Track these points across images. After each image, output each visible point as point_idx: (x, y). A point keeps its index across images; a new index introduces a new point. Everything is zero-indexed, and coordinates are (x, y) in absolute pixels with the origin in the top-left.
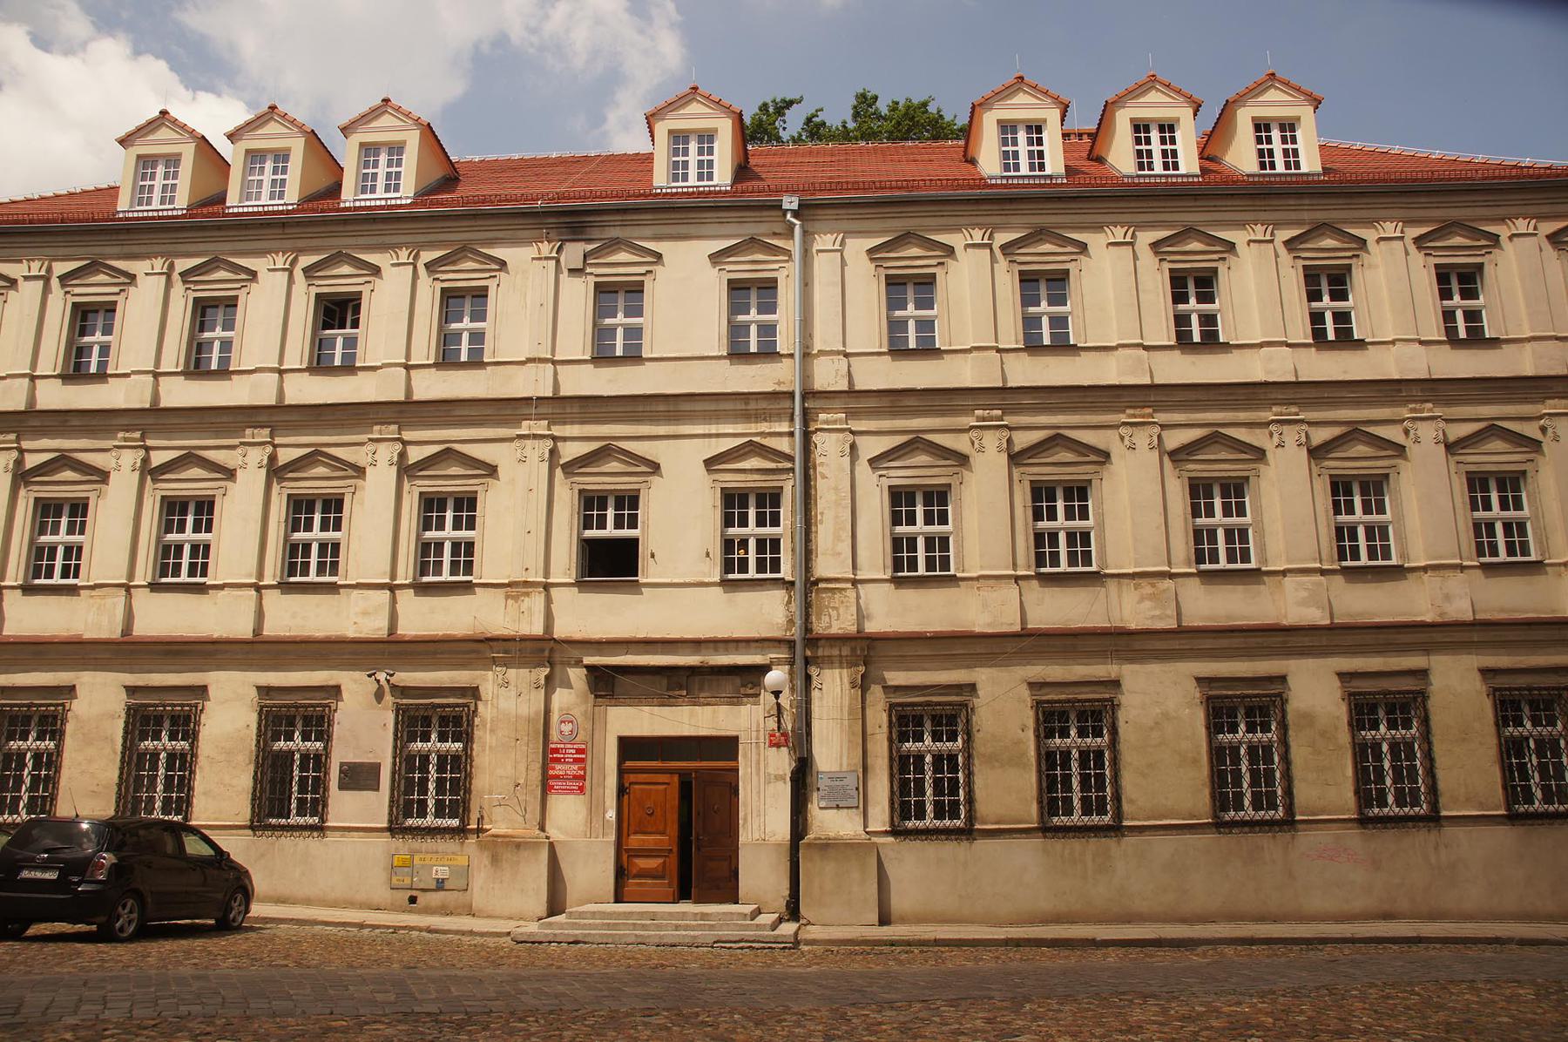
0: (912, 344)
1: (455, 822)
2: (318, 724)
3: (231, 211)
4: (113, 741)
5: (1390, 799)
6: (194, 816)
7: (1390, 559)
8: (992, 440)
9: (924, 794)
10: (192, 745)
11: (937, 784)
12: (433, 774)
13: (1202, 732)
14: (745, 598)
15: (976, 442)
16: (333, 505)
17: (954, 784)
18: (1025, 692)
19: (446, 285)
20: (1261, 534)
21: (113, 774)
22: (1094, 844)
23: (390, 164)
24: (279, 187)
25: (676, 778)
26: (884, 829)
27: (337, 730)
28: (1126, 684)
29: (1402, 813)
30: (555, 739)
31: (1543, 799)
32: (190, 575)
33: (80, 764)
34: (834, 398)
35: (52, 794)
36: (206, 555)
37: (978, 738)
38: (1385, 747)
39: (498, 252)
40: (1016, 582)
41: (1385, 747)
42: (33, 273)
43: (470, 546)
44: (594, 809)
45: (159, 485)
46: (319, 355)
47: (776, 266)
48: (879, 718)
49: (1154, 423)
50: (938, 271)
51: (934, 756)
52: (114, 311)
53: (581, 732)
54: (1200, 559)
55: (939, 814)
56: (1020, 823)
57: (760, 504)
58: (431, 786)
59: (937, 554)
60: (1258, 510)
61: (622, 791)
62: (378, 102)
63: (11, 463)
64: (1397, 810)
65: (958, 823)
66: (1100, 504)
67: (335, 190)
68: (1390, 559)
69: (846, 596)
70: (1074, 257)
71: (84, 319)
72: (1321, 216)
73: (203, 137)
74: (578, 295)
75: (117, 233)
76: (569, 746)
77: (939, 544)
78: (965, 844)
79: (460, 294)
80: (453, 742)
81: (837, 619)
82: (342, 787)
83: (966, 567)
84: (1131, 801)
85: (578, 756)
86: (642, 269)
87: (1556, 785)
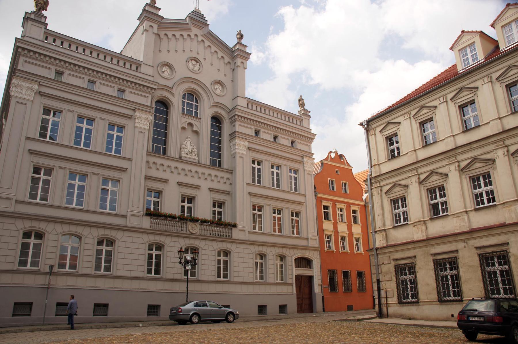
0: (473, 126)
3: (460, 72)
5: (451, 294)
8: (453, 167)
16: (487, 176)
18: (431, 258)
23: (471, 52)
24: (475, 57)
29: (455, 299)
31: (504, 293)
35: (460, 289)
36: (446, 205)
38: (449, 277)
41: (449, 277)
43: (492, 191)
46: (514, 107)
52: (397, 135)
55: (506, 293)
62: (460, 33)
63: (379, 191)
64: (454, 298)
67: (497, 47)
68: (484, 204)
70: (433, 111)
72: (460, 85)
73: (481, 31)
75: (466, 76)
79: (514, 84)
86: (431, 113)
87: (508, 287)
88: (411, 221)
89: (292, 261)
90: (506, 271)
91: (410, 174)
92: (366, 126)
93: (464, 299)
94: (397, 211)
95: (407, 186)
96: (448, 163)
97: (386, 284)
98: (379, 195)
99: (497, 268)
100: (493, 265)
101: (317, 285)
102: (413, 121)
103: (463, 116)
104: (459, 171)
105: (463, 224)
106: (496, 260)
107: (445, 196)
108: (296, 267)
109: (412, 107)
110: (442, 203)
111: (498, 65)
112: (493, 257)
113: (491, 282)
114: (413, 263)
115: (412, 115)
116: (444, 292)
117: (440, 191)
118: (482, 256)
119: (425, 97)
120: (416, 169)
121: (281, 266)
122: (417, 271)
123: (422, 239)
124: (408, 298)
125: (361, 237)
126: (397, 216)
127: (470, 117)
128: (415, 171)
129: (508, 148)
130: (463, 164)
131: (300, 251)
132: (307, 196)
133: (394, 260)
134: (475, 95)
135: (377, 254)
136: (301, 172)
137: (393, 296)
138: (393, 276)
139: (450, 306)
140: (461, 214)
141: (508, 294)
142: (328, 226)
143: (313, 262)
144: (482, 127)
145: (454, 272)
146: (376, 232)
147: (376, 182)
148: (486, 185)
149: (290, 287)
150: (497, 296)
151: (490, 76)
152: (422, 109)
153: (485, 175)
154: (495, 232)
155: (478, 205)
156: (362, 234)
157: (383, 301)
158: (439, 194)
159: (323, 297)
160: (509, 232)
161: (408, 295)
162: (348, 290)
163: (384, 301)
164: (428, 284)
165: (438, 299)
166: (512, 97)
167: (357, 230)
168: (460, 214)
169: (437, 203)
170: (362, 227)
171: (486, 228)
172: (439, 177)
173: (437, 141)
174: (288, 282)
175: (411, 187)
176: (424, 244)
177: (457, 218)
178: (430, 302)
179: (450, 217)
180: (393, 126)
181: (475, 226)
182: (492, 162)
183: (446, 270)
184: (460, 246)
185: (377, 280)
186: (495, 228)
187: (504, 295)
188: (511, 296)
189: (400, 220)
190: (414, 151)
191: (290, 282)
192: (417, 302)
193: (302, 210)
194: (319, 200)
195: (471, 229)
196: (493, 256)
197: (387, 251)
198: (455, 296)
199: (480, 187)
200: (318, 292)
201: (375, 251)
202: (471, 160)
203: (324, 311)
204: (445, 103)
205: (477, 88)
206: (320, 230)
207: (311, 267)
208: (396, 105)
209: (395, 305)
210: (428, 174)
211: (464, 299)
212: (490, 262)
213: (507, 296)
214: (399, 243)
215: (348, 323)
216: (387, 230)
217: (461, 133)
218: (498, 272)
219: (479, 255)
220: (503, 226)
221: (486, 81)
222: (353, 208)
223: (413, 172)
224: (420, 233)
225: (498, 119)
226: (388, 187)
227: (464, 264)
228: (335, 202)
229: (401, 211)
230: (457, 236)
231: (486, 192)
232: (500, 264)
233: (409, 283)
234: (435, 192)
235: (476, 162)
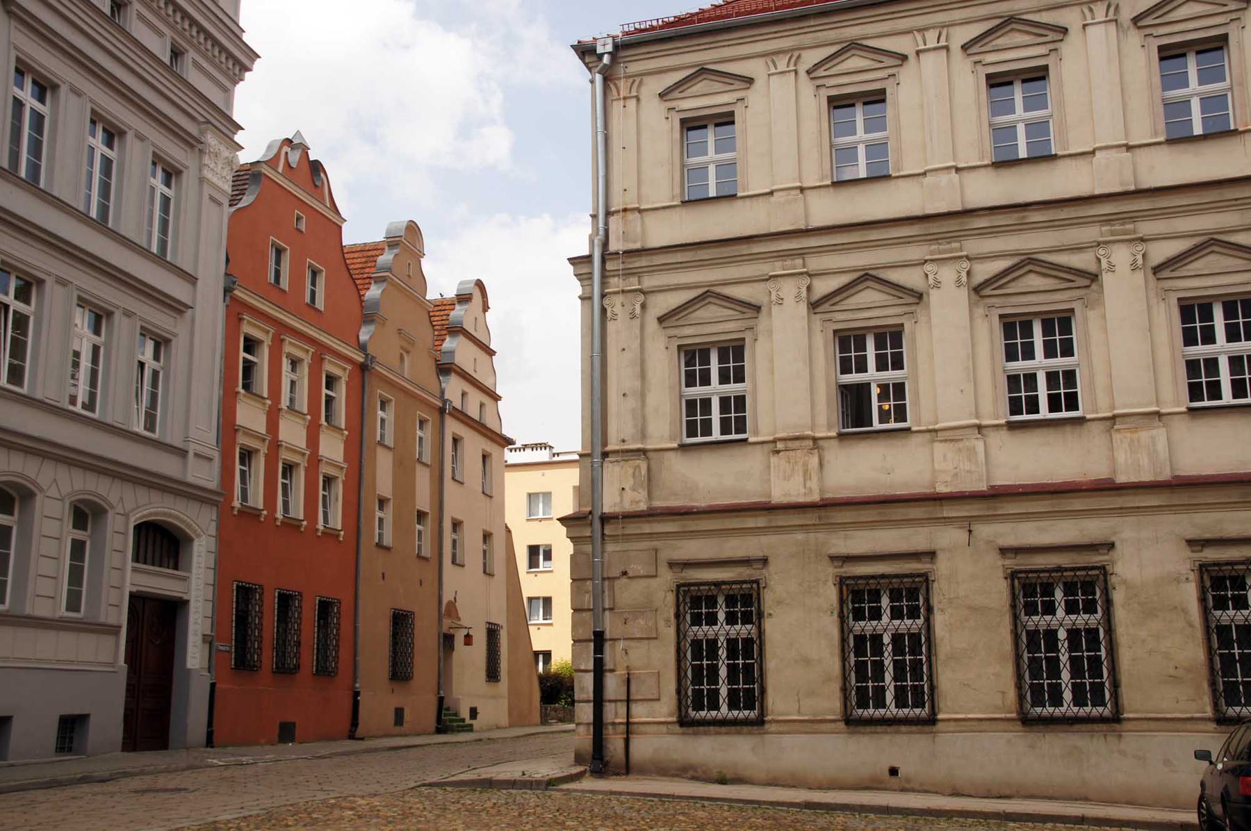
0: (1023, 153)
1: (753, 714)
4: (1185, 611)
6: (769, 712)
7: (1037, 412)
11: (1075, 663)
15: (931, 277)
16: (733, 353)
17: (1095, 663)
18: (830, 572)
19: (992, 70)
21: (1200, 654)
31: (1073, 699)
32: (722, 433)
33: (1143, 641)
43: (741, 401)
49: (961, 257)
50: (1050, 61)
51: (1068, 631)
57: (1048, 329)
58: (723, 672)
59: (699, 418)
68: (1037, 412)
70: (891, 71)
79: (702, 123)
80: (743, 624)
88: (756, 433)
89: (125, 534)
90: (915, 638)
91: (777, 268)
92: (606, 59)
93: (766, 719)
95: (758, 309)
97: (630, 652)
98: (637, 322)
99: (1061, 620)
100: (712, 620)
101: (199, 639)
102: (807, 87)
105: (967, 466)
106: (1059, 595)
108: (136, 559)
109: (811, 35)
111: (653, 58)
112: (1052, 584)
113: (698, 671)
114: (757, 582)
115: (802, 68)
119: (680, 45)
120: (802, 253)
121: (78, 548)
123: (801, 500)
125: (342, 477)
127: (709, 163)
129: (646, 298)
130: (823, 287)
131: (156, 496)
132: (199, 283)
133: (672, 565)
134: (1053, 54)
135: (603, 534)
136: (189, 179)
137: (655, 697)
138: (661, 624)
139: (887, 738)
141: (1087, 706)
142: (250, 416)
143: (191, 547)
144: (739, 203)
145: (742, 630)
146: (605, 455)
147: (628, 273)
148: (724, 379)
149: (108, 641)
150: (1051, 709)
151: (796, 54)
152: (700, 78)
153: (694, 353)
154: (1077, 504)
155: (691, 432)
156: (345, 466)
157: (615, 714)
158: (877, 355)
159: (213, 686)
160: (1122, 511)
162: (285, 669)
163: (616, 714)
164: (807, 661)
167: (332, 448)
169: (866, 387)
170: (347, 443)
171: (1052, 490)
172: (891, 298)
173: (739, 194)
174: (102, 620)
175: (934, 297)
176: (810, 518)
177: (950, 445)
178: (812, 725)
179: (915, 440)
180: (717, 87)
181: (1003, 478)
184: (946, 538)
185: (595, 633)
187: (1074, 706)
188: (1094, 710)
190: (798, 191)
191: (112, 620)
192: (1116, 718)
193: (175, 335)
194: (236, 311)
195: (993, 487)
196: (1051, 580)
197: (647, 528)
199: (706, 381)
200: (197, 667)
201: (597, 524)
202: (1015, 260)
203: (210, 742)
205: (1065, 31)
206: (228, 427)
207: (180, 565)
208: (700, 21)
209: (664, 728)
210: (845, 279)
211: (940, 716)
212: (739, 608)
214: (702, 503)
215: (499, 796)
216: (651, 455)
217: (986, 166)
218: (1062, 635)
219: (1013, 576)
221: (1100, 15)
222: (330, 367)
223: (788, 263)
224: (799, 478)
225: (1124, 149)
227: (950, 601)
228: (282, 329)
229: (717, 394)
230: (942, 505)
231: (721, 399)
232: (1071, 608)
233: (723, 653)
234: (862, 346)
235: (1030, 271)
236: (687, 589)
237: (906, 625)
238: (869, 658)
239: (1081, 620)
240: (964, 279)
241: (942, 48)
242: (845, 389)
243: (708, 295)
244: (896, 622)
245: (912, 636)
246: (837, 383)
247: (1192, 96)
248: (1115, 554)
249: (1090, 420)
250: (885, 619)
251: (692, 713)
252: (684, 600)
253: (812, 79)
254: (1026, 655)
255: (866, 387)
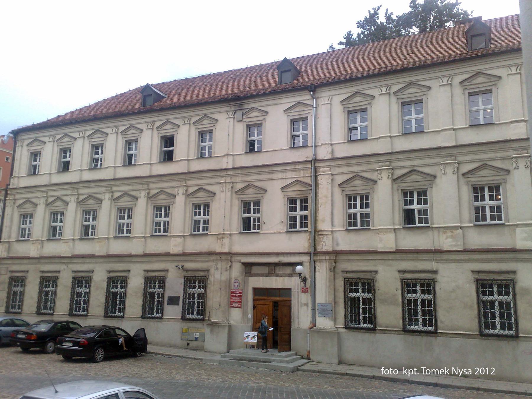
0: (414, 131)
2: (162, 282)
7: (357, 226)
9: (511, 320)
10: (205, 291)
12: (420, 307)
13: (474, 294)
14: (295, 236)
15: (379, 176)
19: (200, 130)
20: (506, 208)
22: (425, 339)
25: (272, 303)
26: (342, 326)
27: (167, 285)
28: (441, 272)
30: (233, 288)
34: (326, 162)
37: (438, 294)
39: (215, 116)
40: (394, 231)
42: (113, 132)
43: (368, 214)
44: (245, 314)
45: (116, 204)
47: (307, 112)
48: (340, 283)
50: (424, 98)
53: (241, 286)
54: (477, 219)
55: (503, 328)
56: (395, 328)
57: (419, 195)
60: (506, 198)
61: (254, 307)
64: (196, 316)
65: (511, 332)
66: (432, 198)
68: (357, 226)
69: (328, 237)
71: (130, 145)
74: (240, 129)
76: (237, 291)
77: (366, 217)
78: (373, 335)
79: (298, 120)
81: (325, 245)
82: (169, 304)
83: (375, 225)
84: (442, 322)
85: (240, 294)
88: (32, 238)
94: (121, 221)
96: (71, 194)
100: (415, 292)
103: (200, 142)
104: (147, 198)
107: (208, 215)
110: (254, 219)
113: (410, 311)
116: (189, 310)
117: (205, 208)
118: (187, 279)
122: (26, 284)
124: (193, 314)
126: (121, 226)
128: (45, 193)
129: (113, 194)
130: (399, 173)
140: (69, 240)
151: (118, 127)
160: (97, 263)
161: (193, 310)
165: (182, 317)
166: (293, 132)
168: (67, 240)
172: (94, 201)
173: (368, 138)
175: (380, 182)
177: (66, 244)
180: (39, 144)
181: (77, 253)
182: (213, 195)
183: (194, 287)
184: (171, 266)
186: (89, 257)
189: (123, 231)
192: (516, 337)
198: (198, 314)
199: (355, 207)
204: (151, 130)
205: (500, 78)
211: (125, 316)
213: (425, 328)
220: (93, 256)
226: (21, 202)
231: (127, 224)
232: (423, 292)
234: (200, 209)
236: (348, 280)
237: (426, 296)
238: (505, 311)
239: (426, 296)
240: (390, 176)
241: (518, 73)
242: (244, 219)
243: (356, 176)
244: (423, 295)
245: (428, 301)
246: (403, 209)
247: (480, 110)
248: (94, 273)
249: (95, 239)
250: (418, 294)
251: (408, 327)
252: (347, 283)
253: (122, 135)
254: (482, 311)
255: (413, 211)
